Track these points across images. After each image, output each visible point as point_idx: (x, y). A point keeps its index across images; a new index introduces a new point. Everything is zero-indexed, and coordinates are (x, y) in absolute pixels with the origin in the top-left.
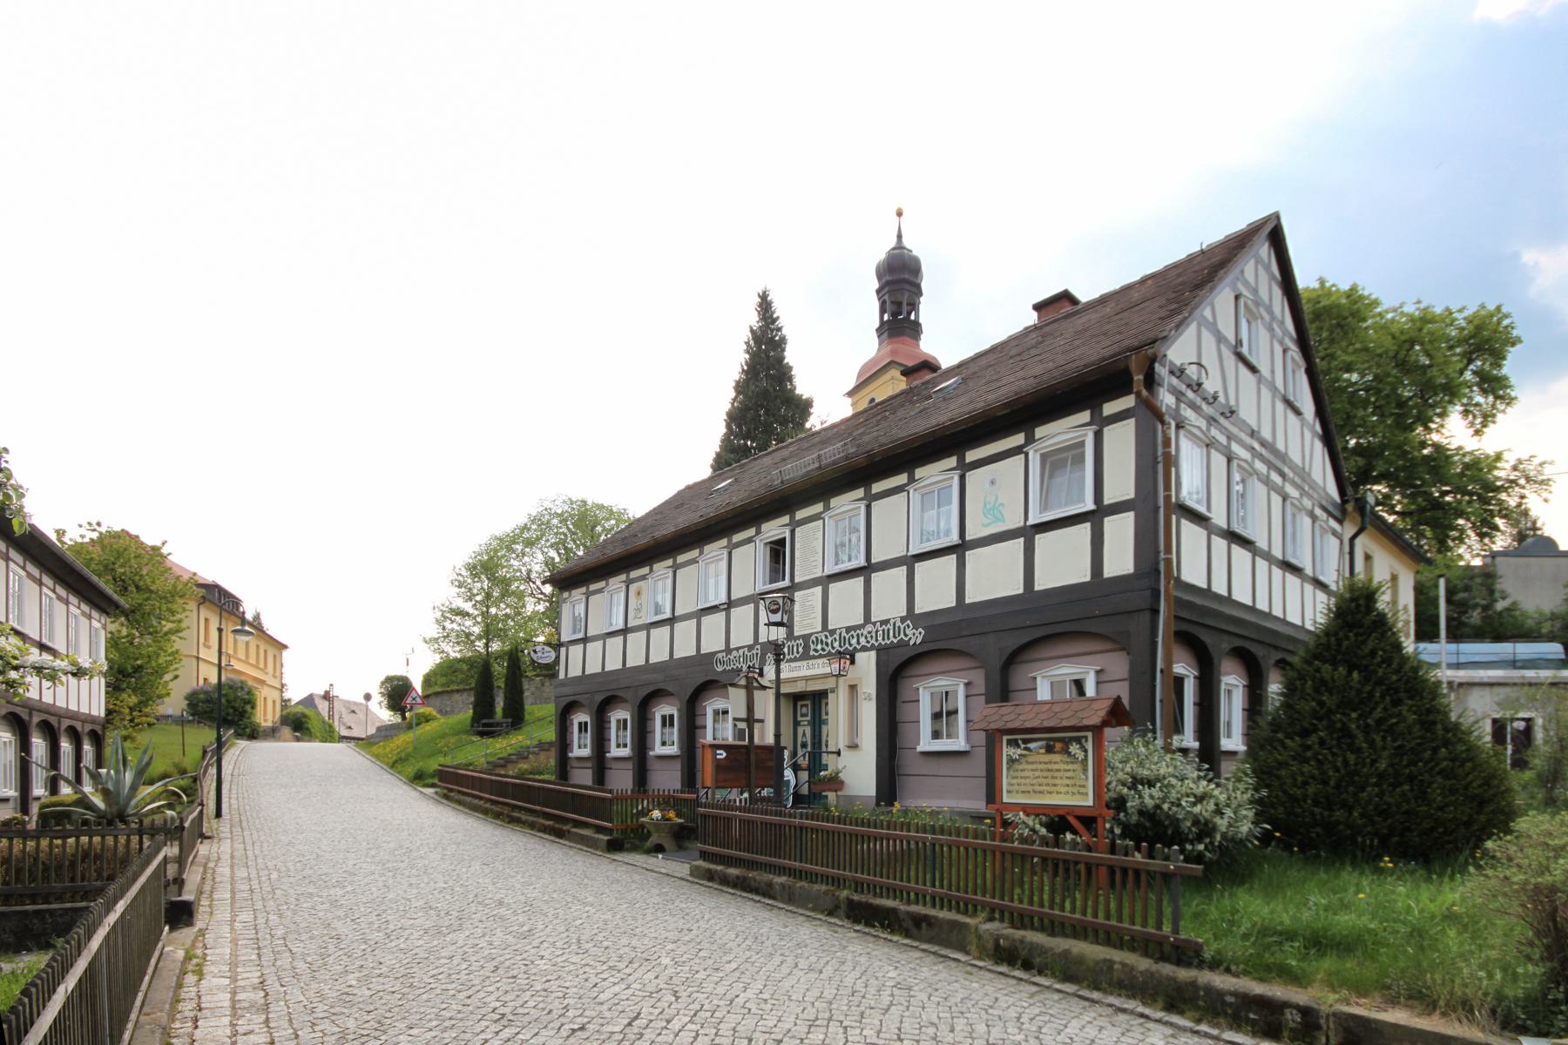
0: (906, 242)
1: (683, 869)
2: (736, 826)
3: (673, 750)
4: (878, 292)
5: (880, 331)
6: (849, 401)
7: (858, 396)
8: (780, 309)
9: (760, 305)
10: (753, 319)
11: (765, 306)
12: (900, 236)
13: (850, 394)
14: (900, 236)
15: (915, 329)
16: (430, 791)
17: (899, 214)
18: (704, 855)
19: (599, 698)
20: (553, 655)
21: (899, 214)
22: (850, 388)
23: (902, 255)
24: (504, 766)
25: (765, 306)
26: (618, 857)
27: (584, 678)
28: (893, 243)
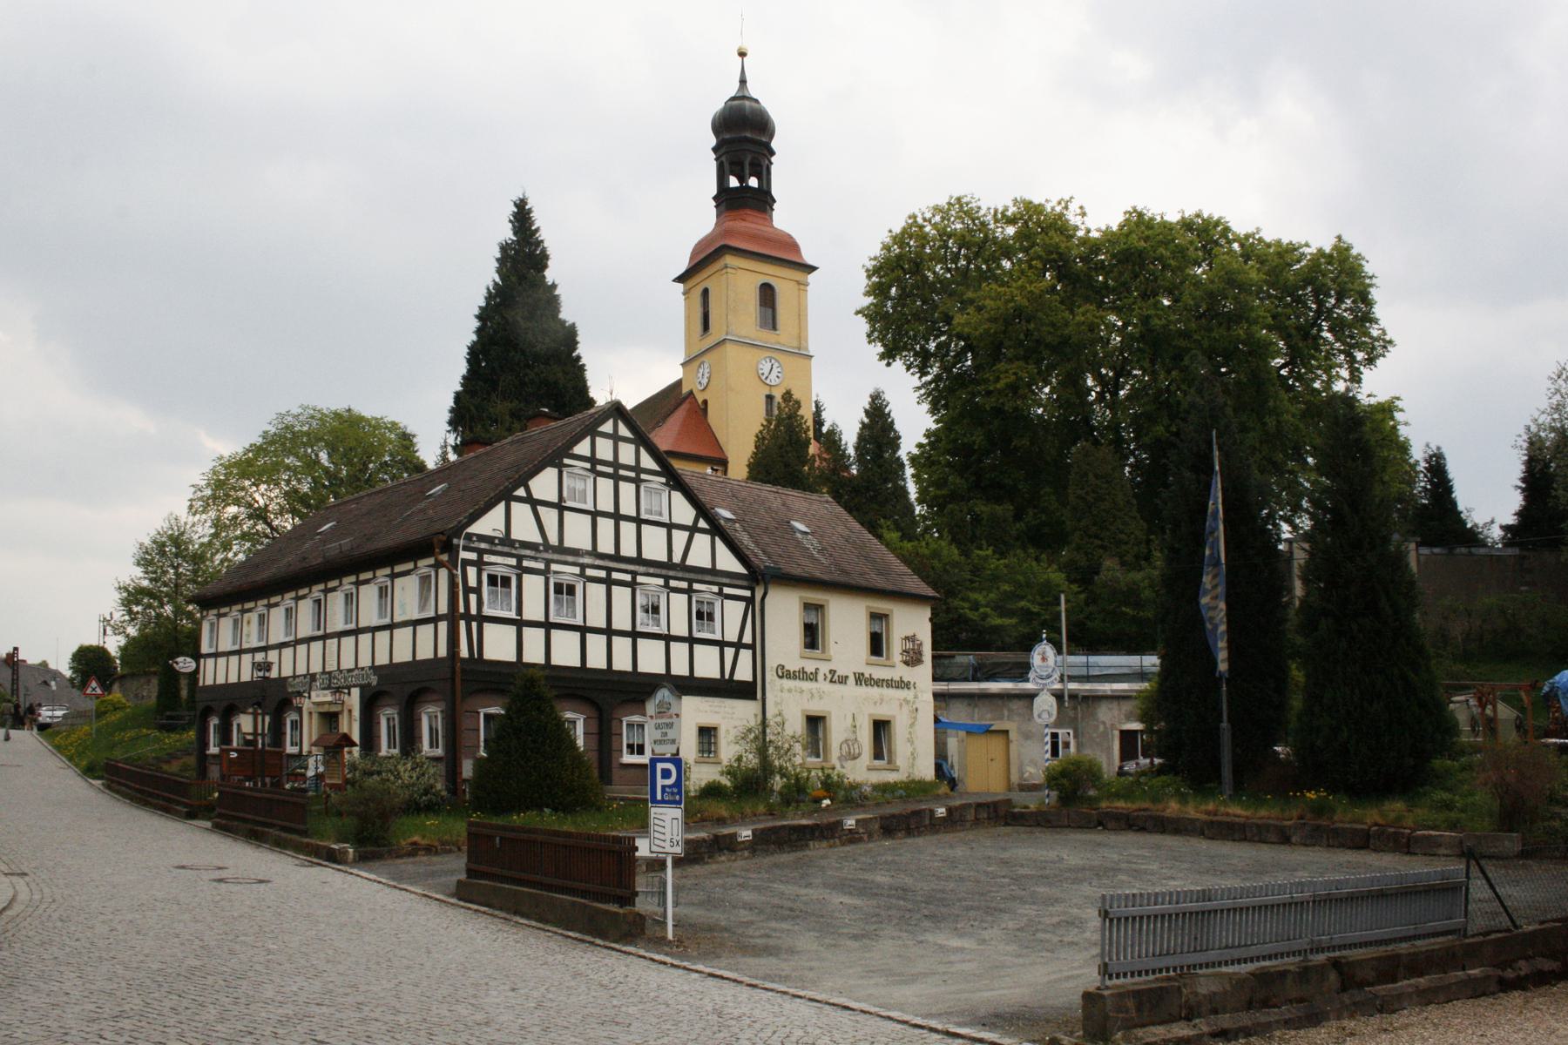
0: (753, 90)
1: (208, 824)
2: (683, 910)
3: (439, 752)
4: (715, 150)
5: (450, 423)
6: (680, 286)
7: (692, 282)
8: (540, 219)
9: (515, 215)
10: (507, 233)
11: (522, 217)
12: (743, 82)
13: (680, 279)
14: (743, 82)
15: (763, 200)
16: (98, 783)
17: (742, 54)
18: (220, 816)
19: (225, 704)
20: (194, 665)
21: (742, 54)
22: (682, 266)
23: (740, 109)
24: (168, 762)
25: (522, 217)
26: (195, 822)
27: (215, 687)
28: (732, 89)
